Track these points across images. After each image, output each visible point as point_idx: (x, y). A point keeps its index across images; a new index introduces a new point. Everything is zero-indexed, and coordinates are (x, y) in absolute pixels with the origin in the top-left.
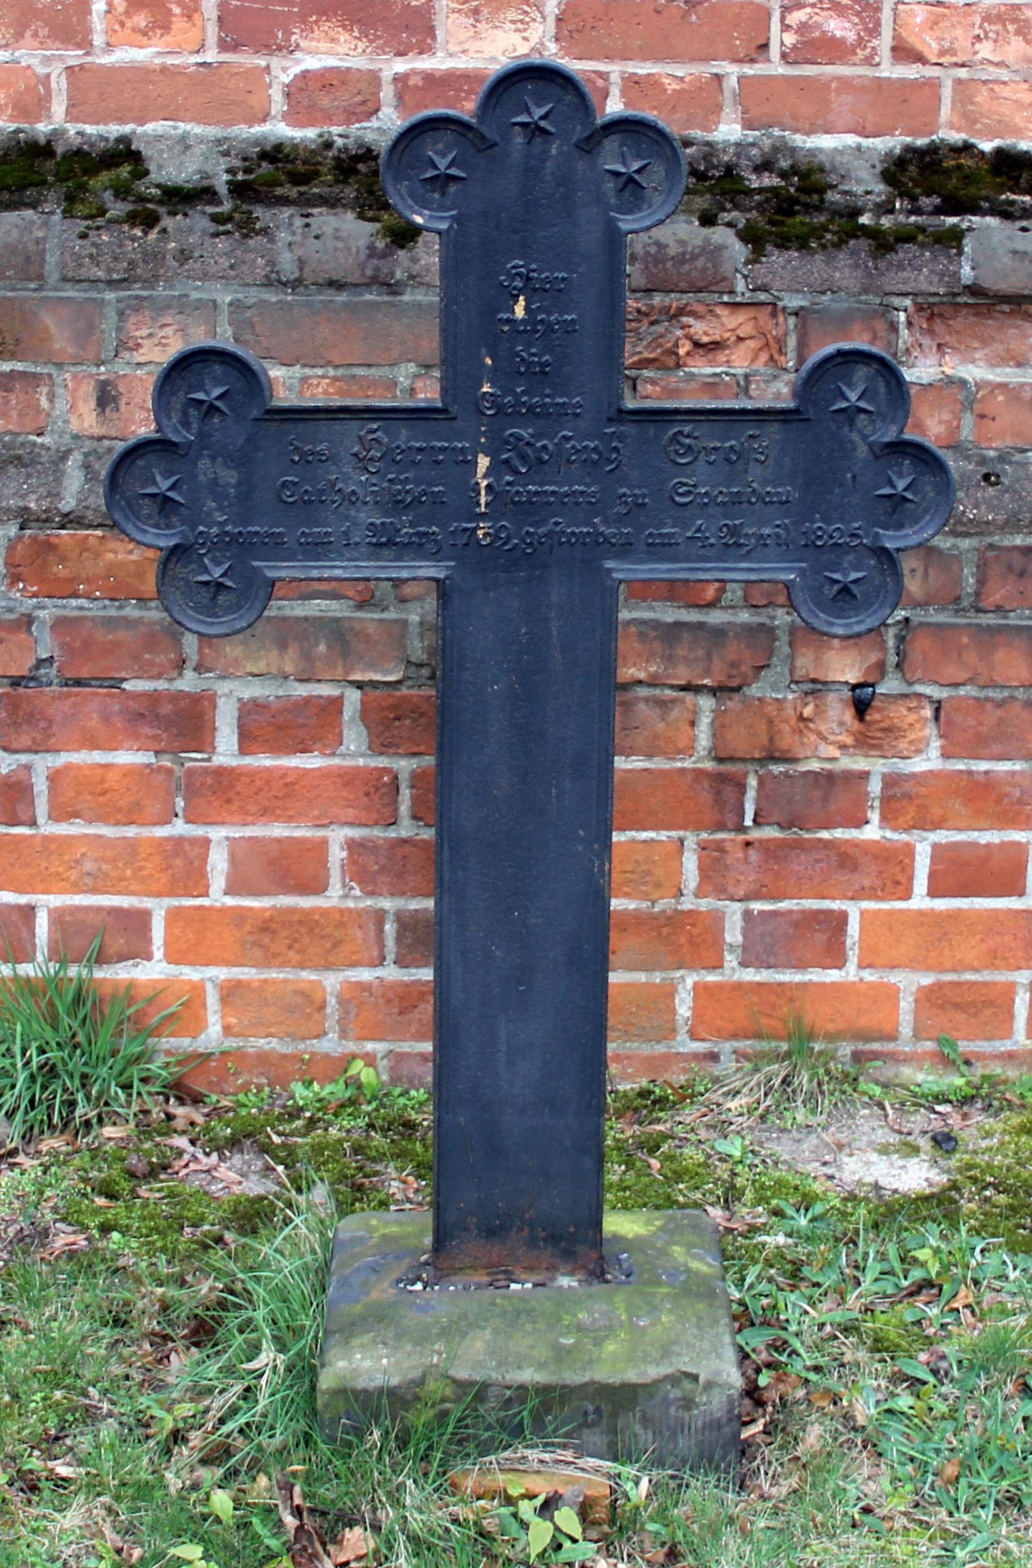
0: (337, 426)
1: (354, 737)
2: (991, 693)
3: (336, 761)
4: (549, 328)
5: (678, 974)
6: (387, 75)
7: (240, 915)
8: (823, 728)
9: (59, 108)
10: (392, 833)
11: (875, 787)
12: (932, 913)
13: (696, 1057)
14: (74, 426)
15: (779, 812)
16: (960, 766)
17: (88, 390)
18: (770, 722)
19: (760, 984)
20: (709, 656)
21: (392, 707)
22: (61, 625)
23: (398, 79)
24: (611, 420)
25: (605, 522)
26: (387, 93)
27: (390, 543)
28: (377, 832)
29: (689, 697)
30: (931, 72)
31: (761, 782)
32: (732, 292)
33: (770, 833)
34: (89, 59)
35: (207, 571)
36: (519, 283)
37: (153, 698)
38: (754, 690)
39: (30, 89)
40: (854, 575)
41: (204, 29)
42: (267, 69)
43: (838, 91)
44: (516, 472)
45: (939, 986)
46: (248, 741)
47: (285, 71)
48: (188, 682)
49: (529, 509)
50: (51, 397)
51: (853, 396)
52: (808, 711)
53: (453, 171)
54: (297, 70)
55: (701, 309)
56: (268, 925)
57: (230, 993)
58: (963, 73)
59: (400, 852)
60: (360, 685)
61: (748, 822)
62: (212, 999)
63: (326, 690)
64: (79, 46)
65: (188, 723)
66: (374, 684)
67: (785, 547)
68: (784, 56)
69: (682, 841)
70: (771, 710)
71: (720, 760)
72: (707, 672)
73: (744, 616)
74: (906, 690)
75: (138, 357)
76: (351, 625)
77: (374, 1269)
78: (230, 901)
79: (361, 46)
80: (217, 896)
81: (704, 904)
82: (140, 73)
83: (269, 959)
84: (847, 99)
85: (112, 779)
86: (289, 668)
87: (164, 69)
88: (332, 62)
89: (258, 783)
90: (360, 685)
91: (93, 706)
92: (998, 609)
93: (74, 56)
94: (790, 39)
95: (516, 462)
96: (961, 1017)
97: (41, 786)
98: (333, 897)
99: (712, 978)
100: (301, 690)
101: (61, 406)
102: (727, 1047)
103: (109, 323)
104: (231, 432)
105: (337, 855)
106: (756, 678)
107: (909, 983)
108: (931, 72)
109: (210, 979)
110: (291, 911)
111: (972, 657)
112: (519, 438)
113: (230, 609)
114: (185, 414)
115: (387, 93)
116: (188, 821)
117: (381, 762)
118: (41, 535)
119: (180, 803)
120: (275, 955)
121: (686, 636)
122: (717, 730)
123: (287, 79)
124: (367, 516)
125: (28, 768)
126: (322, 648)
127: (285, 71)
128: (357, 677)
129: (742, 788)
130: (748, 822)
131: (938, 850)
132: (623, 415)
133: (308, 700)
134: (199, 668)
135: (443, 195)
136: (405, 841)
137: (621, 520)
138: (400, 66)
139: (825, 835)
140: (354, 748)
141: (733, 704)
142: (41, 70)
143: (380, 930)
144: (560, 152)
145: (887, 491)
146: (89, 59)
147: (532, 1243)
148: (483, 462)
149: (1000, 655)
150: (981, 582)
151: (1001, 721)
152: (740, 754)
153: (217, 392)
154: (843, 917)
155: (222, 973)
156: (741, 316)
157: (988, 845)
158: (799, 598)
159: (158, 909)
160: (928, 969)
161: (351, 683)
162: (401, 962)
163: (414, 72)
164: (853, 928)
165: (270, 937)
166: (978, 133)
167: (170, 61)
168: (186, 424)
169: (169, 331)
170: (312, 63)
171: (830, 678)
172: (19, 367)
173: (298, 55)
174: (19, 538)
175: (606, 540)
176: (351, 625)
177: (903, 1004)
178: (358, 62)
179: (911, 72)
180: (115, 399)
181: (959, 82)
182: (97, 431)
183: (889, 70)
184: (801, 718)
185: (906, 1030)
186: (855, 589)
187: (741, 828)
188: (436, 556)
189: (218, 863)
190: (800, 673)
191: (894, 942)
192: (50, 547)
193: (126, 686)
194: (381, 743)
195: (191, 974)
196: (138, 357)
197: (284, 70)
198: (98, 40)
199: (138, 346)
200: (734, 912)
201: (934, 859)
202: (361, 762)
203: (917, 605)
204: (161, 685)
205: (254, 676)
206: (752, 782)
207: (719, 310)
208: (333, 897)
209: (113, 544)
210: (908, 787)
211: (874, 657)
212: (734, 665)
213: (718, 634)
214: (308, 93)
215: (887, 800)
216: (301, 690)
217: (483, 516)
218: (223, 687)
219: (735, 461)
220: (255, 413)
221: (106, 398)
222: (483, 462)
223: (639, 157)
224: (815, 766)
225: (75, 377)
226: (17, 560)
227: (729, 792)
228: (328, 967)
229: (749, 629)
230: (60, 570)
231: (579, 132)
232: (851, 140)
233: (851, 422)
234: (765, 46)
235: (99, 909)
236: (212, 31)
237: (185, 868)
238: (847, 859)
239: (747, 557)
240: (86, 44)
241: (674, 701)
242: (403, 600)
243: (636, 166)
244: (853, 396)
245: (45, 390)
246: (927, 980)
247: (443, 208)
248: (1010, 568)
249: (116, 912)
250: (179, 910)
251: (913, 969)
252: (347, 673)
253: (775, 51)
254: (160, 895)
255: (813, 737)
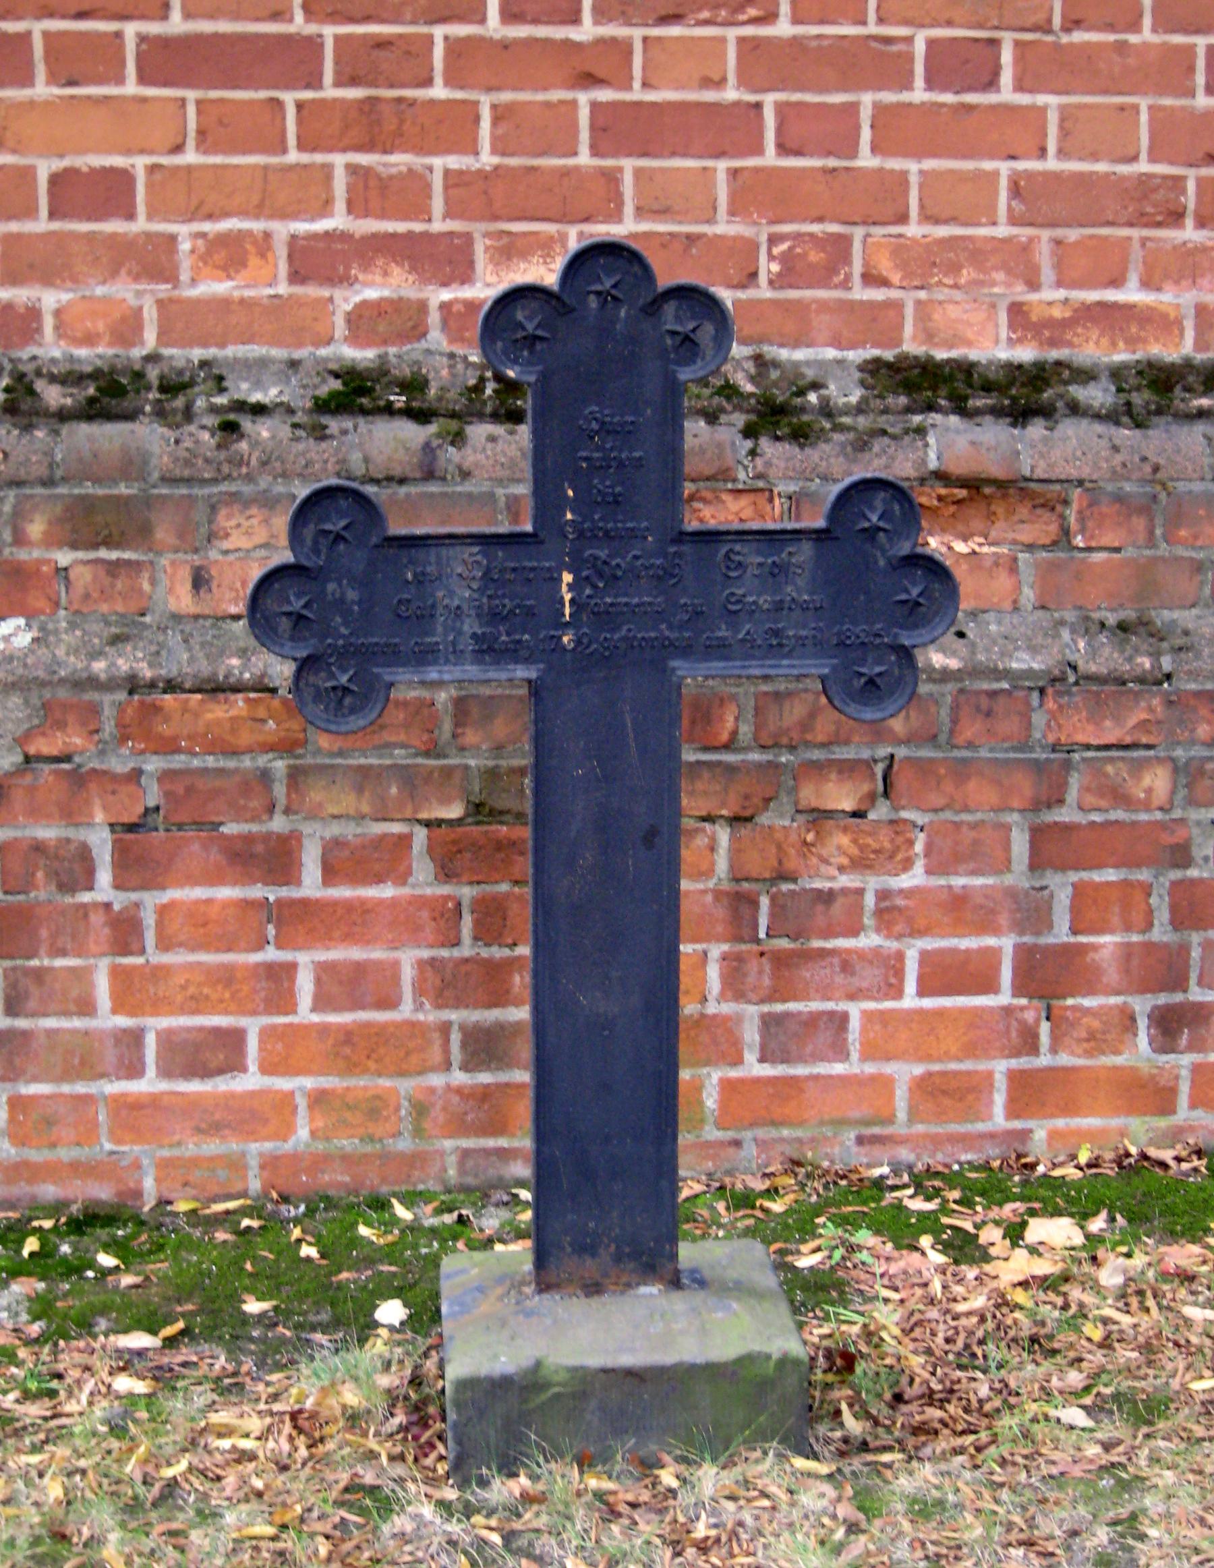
0: (444, 551)
1: (422, 870)
2: (965, 817)
3: (405, 891)
4: (621, 465)
5: (705, 1071)
6: (434, 304)
7: (324, 1029)
8: (824, 852)
9: (150, 338)
10: (456, 953)
11: (870, 900)
12: (921, 1012)
13: (721, 1144)
14: (173, 605)
15: (786, 930)
16: (942, 881)
17: (185, 575)
18: (779, 847)
19: (776, 1078)
20: (726, 790)
21: (454, 842)
22: (166, 776)
23: (445, 307)
24: (673, 541)
25: (671, 627)
26: (434, 318)
27: (491, 649)
28: (445, 953)
29: (707, 825)
30: (894, 294)
31: (773, 899)
32: (735, 480)
33: (784, 943)
34: (176, 293)
35: (332, 676)
36: (595, 426)
37: (249, 839)
38: (764, 819)
39: (124, 320)
40: (878, 669)
41: (276, 266)
42: (331, 299)
43: (818, 312)
44: (595, 587)
45: (930, 1074)
46: (330, 873)
47: (346, 300)
48: (278, 824)
49: (606, 618)
50: (153, 582)
51: (874, 518)
52: (810, 837)
53: (540, 333)
54: (357, 299)
55: (708, 495)
56: (348, 1035)
57: (318, 1099)
58: (922, 295)
59: (463, 969)
60: (428, 824)
61: (762, 935)
62: (301, 1102)
63: (396, 828)
64: (167, 281)
65: (278, 860)
66: (440, 822)
67: (819, 647)
68: (771, 282)
69: (705, 953)
70: (778, 836)
71: (737, 880)
72: (723, 805)
73: (755, 756)
74: (893, 816)
75: (226, 545)
76: (462, 713)
77: (481, 1289)
78: (316, 1018)
79: (411, 278)
80: (305, 1013)
81: (727, 1008)
82: (223, 304)
83: (352, 1068)
84: (825, 318)
85: (214, 912)
86: (365, 808)
87: (242, 301)
88: (386, 293)
89: (340, 912)
90: (428, 824)
91: (195, 849)
92: (970, 745)
93: (163, 289)
94: (775, 267)
95: (594, 579)
96: (947, 1102)
97: (149, 919)
98: (406, 1011)
99: (734, 1073)
100: (379, 828)
101: (161, 591)
102: (747, 1135)
103: (200, 514)
104: (355, 558)
105: (408, 974)
106: (766, 809)
107: (904, 1073)
108: (894, 294)
109: (301, 1089)
110: (368, 1025)
111: (948, 787)
112: (596, 558)
113: (353, 711)
114: (316, 542)
115: (434, 318)
116: (279, 947)
117: (445, 890)
118: (148, 699)
119: (271, 930)
120: (355, 1065)
121: (706, 774)
122: (736, 852)
123: (349, 308)
124: (470, 626)
125: (137, 905)
126: (394, 790)
127: (346, 300)
128: (424, 815)
129: (755, 904)
130: (762, 935)
131: (925, 956)
132: (682, 537)
133: (384, 837)
134: (287, 811)
135: (531, 352)
136: (466, 961)
137: (682, 627)
138: (446, 295)
139: (830, 944)
140: (423, 879)
141: (745, 831)
142: (132, 301)
143: (447, 1041)
144: (628, 315)
145: (903, 597)
146: (176, 293)
147: (618, 1258)
148: (567, 578)
149: (972, 785)
150: (955, 721)
151: (976, 842)
152: (754, 875)
153: (343, 523)
154: (844, 1017)
155: (309, 1082)
156: (744, 501)
157: (967, 951)
158: (833, 689)
159: (253, 1026)
160: (921, 1059)
161: (419, 821)
162: (465, 1068)
163: (456, 300)
164: (855, 1023)
165: (353, 1050)
166: (936, 345)
167: (248, 293)
168: (317, 552)
169: (254, 521)
170: (372, 294)
171: (830, 806)
172: (127, 555)
173: (357, 287)
174: (129, 703)
175: (672, 644)
176: (462, 713)
177: (898, 1092)
178: (411, 291)
179: (877, 295)
180: (208, 582)
181: (918, 303)
182: (193, 610)
183: (861, 293)
184: (805, 843)
185: (902, 1115)
186: (878, 681)
187: (758, 941)
188: (527, 661)
189: (305, 984)
190: (803, 804)
191: (887, 1036)
192: (157, 709)
193: (224, 829)
194: (446, 873)
195: (284, 1084)
196: (226, 545)
197: (346, 300)
198: (184, 277)
199: (227, 535)
200: (752, 1012)
201: (922, 963)
202: (429, 891)
203: (900, 742)
204: (254, 828)
205: (335, 817)
206: (765, 902)
207: (724, 497)
208: (406, 1011)
209: (212, 706)
210: (900, 902)
211: (866, 787)
212: (747, 797)
213: (731, 769)
214: (363, 321)
215: (879, 913)
216: (379, 828)
217: (567, 624)
218: (307, 828)
219: (778, 572)
220: (374, 540)
221: (200, 581)
222: (567, 578)
223: (693, 318)
224: (818, 884)
225: (173, 563)
226: (127, 720)
227: (745, 910)
228: (402, 1074)
229: (759, 766)
230: (164, 729)
231: (644, 299)
232: (831, 353)
233: (873, 539)
234: (754, 275)
235: (201, 1029)
236: (283, 268)
237: (276, 985)
238: (847, 961)
239: (789, 655)
240: (172, 278)
241: (697, 830)
242: (462, 749)
243: (691, 326)
244: (874, 518)
245: (146, 575)
246: (918, 1070)
247: (530, 363)
248: (978, 709)
249: (217, 1031)
250: (274, 1027)
251: (907, 1060)
252: (416, 811)
253: (763, 278)
254: (254, 1013)
255: (815, 860)
